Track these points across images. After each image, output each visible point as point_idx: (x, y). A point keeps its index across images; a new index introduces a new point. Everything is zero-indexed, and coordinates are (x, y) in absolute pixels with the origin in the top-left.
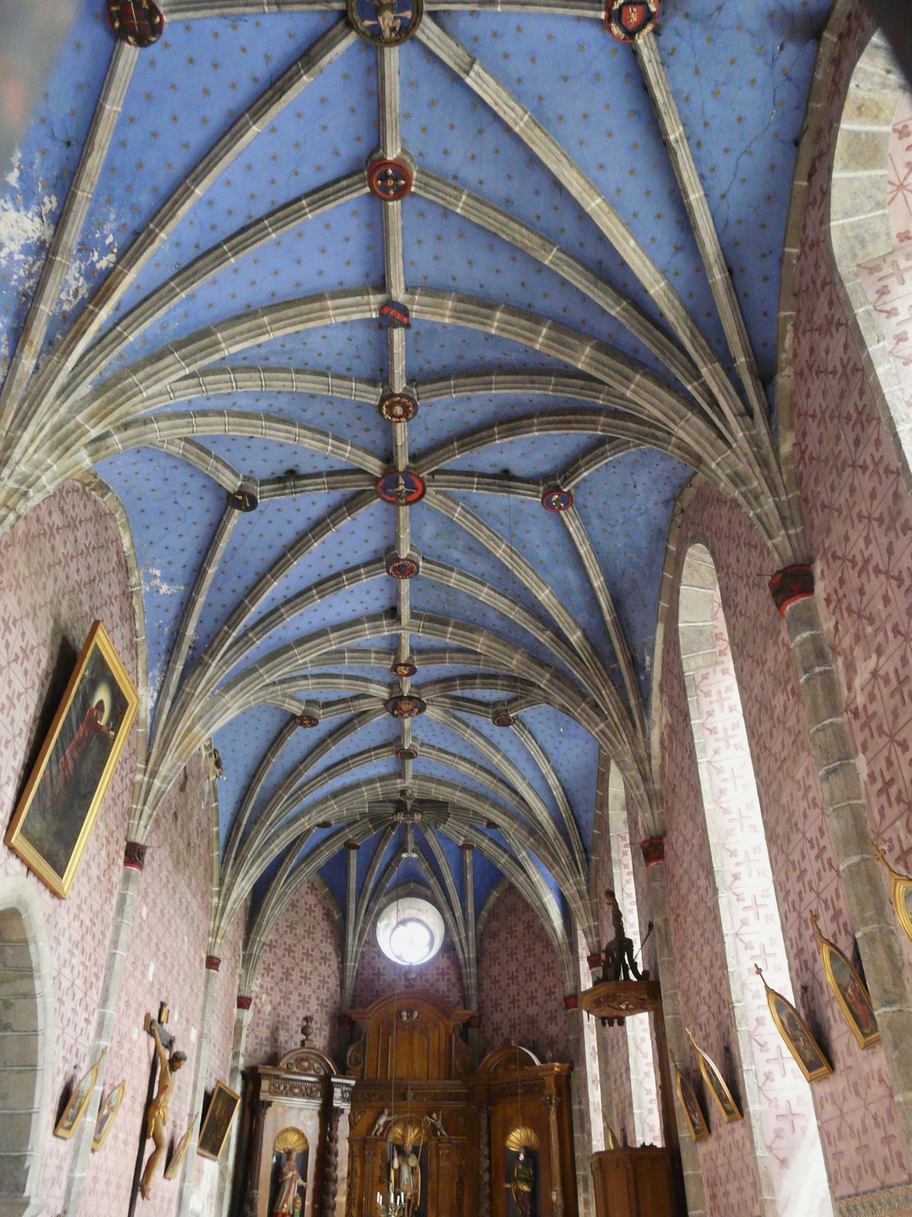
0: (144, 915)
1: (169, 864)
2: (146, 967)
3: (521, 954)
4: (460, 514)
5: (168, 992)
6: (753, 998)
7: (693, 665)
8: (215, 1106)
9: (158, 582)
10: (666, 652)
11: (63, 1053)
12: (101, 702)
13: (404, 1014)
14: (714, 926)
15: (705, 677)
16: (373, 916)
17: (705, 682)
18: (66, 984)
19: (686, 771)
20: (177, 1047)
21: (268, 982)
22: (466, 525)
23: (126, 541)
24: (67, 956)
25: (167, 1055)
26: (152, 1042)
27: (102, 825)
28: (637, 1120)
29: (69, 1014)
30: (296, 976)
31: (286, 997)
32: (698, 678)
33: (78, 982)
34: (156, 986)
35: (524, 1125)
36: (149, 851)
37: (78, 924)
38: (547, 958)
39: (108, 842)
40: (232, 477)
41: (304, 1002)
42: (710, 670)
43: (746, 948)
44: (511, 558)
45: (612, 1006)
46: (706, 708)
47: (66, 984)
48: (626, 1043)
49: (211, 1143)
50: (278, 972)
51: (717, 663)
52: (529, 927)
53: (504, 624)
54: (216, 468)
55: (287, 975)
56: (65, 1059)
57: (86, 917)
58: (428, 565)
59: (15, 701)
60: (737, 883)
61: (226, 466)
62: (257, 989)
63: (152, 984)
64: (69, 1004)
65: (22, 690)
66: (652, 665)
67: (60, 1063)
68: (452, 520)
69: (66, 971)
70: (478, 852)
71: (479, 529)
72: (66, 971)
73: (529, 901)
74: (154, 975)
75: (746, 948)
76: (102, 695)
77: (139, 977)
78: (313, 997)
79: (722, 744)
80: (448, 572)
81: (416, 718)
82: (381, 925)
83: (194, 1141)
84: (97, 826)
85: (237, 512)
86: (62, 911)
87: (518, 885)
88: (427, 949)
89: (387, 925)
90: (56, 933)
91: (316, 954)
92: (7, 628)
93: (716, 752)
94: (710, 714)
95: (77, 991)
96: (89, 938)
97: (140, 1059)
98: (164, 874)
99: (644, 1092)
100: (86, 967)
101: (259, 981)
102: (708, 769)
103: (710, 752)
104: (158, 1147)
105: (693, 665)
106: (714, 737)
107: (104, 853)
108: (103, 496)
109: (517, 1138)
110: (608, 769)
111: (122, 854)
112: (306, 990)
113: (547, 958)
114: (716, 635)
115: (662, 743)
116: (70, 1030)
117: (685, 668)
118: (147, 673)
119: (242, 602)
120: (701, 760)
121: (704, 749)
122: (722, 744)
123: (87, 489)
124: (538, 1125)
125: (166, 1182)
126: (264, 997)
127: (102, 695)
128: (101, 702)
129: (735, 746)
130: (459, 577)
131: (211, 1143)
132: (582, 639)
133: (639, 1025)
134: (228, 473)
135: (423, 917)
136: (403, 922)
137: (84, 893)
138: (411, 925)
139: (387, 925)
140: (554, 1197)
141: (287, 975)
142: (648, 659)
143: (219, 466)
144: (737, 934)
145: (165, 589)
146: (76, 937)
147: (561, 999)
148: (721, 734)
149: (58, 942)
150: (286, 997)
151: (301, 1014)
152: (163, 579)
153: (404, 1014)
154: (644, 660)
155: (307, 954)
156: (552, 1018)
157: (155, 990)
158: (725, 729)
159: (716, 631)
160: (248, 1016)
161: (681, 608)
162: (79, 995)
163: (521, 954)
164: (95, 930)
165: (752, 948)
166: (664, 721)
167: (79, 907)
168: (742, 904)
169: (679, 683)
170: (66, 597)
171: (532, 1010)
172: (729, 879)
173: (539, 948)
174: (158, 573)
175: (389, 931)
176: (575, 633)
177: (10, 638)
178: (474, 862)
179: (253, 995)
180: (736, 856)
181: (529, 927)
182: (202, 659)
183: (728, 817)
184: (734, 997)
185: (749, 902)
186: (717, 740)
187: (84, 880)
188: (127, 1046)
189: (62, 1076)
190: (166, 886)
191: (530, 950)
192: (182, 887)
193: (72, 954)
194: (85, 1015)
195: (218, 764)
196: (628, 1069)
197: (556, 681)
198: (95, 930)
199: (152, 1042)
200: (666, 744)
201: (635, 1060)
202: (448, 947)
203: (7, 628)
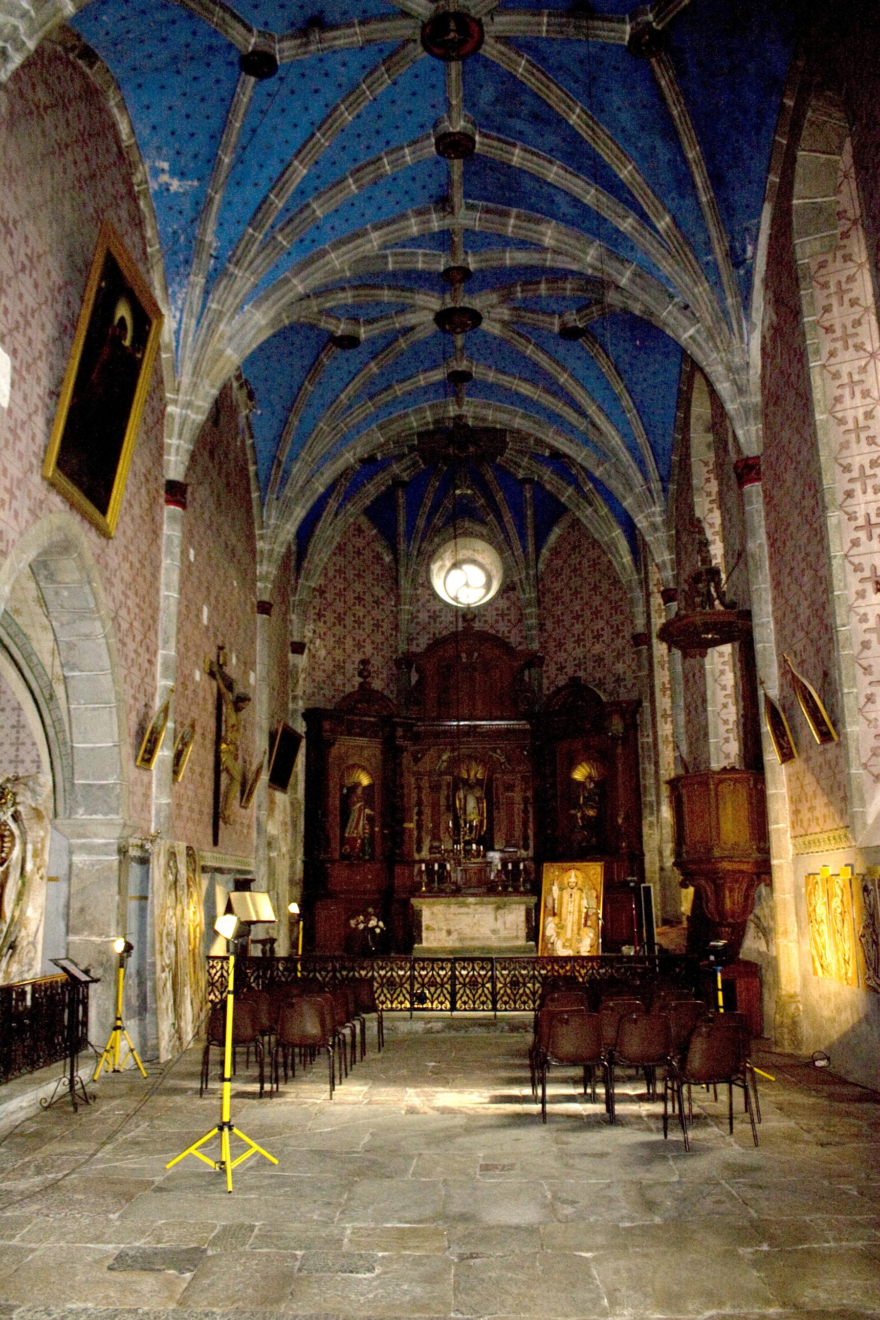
0: (192, 558)
1: (211, 504)
2: (200, 611)
3: (586, 593)
4: (526, 70)
5: (224, 636)
6: (860, 621)
7: (808, 251)
8: (283, 745)
9: (165, 178)
10: (773, 238)
11: (132, 692)
12: (122, 319)
13: (464, 655)
14: (819, 549)
15: (822, 265)
16: (427, 558)
17: (823, 271)
18: (125, 626)
19: (793, 378)
20: (239, 689)
21: (321, 628)
22: (532, 83)
23: (124, 128)
24: (122, 598)
25: (230, 697)
26: (214, 684)
27: (138, 461)
28: (712, 749)
29: (133, 655)
30: (349, 620)
31: (340, 642)
32: (814, 267)
33: (135, 624)
34: (211, 630)
35: (587, 760)
36: (190, 489)
37: (128, 565)
38: (615, 596)
39: (147, 480)
40: (244, 31)
41: (359, 646)
42: (829, 257)
43: (855, 571)
44: (588, 126)
45: (689, 640)
46: (821, 302)
47: (125, 626)
48: (703, 676)
49: (280, 778)
50: (330, 617)
51: (839, 248)
52: (595, 564)
53: (577, 211)
54: (223, 19)
55: (340, 619)
56: (135, 698)
57: (134, 558)
58: (486, 141)
59: (29, 318)
60: (850, 501)
61: (234, 16)
62: (310, 635)
63: (207, 628)
64: (131, 646)
65: (35, 306)
66: (754, 257)
67: (132, 702)
68: (514, 77)
69: (123, 612)
70: (538, 486)
71: (548, 87)
72: (123, 612)
73: (596, 536)
74: (209, 619)
75: (855, 571)
76: (123, 311)
77: (195, 620)
78: (368, 641)
79: (839, 345)
80: (509, 148)
81: (470, 333)
82: (435, 567)
83: (265, 777)
84: (133, 462)
85: (253, 79)
86: (110, 551)
87: (584, 521)
88: (483, 591)
89: (441, 567)
90: (108, 574)
91: (368, 598)
92: (9, 232)
93: (832, 354)
94: (827, 309)
95: (136, 632)
96: (140, 579)
97: (204, 699)
98: (206, 516)
99: (720, 722)
100: (142, 610)
101: (312, 626)
102: (821, 374)
103: (825, 354)
104: (232, 778)
105: (808, 251)
106: (831, 336)
107: (143, 491)
108: (91, 66)
109: (579, 774)
110: (690, 387)
111: (162, 492)
112: (360, 634)
113: (615, 596)
114: (839, 214)
115: (763, 349)
116: (135, 670)
117: (799, 255)
118: (166, 289)
119: (267, 197)
120: (814, 364)
121: (817, 352)
122: (839, 345)
123: (71, 56)
124: (602, 757)
125: (243, 811)
126: (318, 641)
127: (123, 311)
128: (122, 319)
129: (855, 346)
130: (522, 154)
131: (280, 778)
132: (671, 225)
133: (721, 661)
134: (238, 26)
135: (479, 557)
136: (456, 565)
137: (129, 533)
138: (467, 568)
139: (441, 567)
140: (620, 821)
141: (340, 619)
142: (750, 248)
143: (227, 17)
144: (846, 556)
145: (176, 185)
146: (128, 578)
147: (628, 637)
148: (838, 333)
149: (112, 584)
150: (340, 642)
151: (358, 657)
152: (173, 173)
153: (464, 655)
154: (744, 251)
155: (359, 598)
156: (619, 656)
157: (211, 634)
158: (844, 327)
159: (840, 208)
160: (301, 661)
161: (797, 180)
162: (139, 638)
163: (586, 593)
164: (145, 571)
165: (862, 570)
166: (767, 322)
167: (126, 547)
168: (853, 524)
169: (790, 274)
170: (67, 195)
171: (598, 648)
172: (840, 497)
173: (605, 586)
174: (165, 165)
175: (443, 574)
176: (663, 218)
177: (13, 243)
178: (534, 497)
179: (306, 640)
180: (850, 471)
181: (595, 564)
182: (227, 269)
183: (843, 428)
184: (839, 622)
185: (861, 521)
186: (834, 340)
187: (127, 519)
188: (191, 687)
189: (134, 713)
190: (209, 527)
191: (595, 588)
192: (226, 528)
193: (127, 597)
194: (147, 657)
195: (251, 396)
196: (704, 701)
197: (638, 280)
198: (145, 571)
199: (214, 684)
200: (768, 349)
201: (714, 694)
202: (507, 589)
203: (9, 232)
